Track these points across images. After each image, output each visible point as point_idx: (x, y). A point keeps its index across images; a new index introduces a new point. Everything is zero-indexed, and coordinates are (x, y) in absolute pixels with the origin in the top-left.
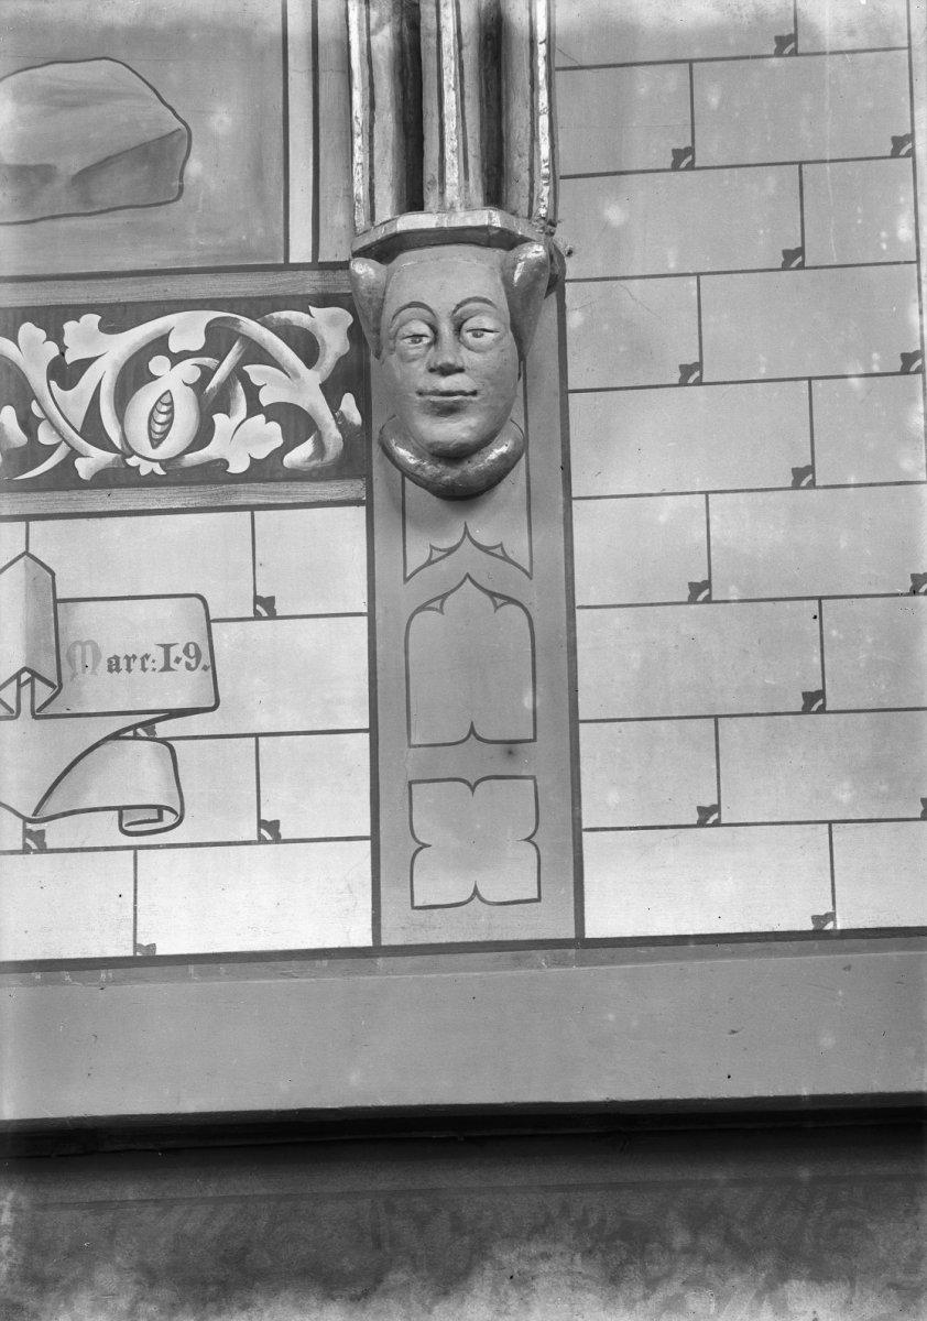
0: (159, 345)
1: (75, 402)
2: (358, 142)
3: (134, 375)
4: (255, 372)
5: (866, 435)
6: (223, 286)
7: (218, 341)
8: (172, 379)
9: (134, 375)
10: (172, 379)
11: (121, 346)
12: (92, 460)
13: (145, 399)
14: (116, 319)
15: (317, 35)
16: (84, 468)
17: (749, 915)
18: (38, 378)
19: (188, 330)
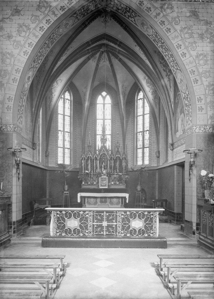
0: (197, 127)
1: (207, 129)
2: (166, 91)
3: (196, 129)
4: (201, 129)
5: (206, 213)
6: (64, 148)
7: (200, 127)
8: (198, 129)
9: (196, 129)
10: (198, 129)
11: (195, 128)
12: (195, 132)
13: (210, 130)
14: (195, 126)
15: (128, 32)
16: (194, 132)
17: (75, 125)
18: (206, 128)
19: (198, 127)
